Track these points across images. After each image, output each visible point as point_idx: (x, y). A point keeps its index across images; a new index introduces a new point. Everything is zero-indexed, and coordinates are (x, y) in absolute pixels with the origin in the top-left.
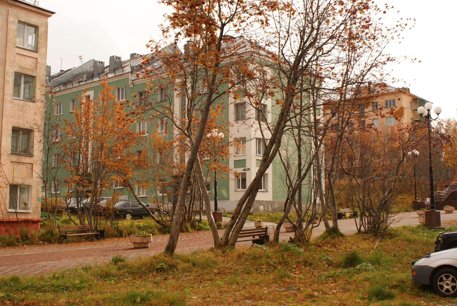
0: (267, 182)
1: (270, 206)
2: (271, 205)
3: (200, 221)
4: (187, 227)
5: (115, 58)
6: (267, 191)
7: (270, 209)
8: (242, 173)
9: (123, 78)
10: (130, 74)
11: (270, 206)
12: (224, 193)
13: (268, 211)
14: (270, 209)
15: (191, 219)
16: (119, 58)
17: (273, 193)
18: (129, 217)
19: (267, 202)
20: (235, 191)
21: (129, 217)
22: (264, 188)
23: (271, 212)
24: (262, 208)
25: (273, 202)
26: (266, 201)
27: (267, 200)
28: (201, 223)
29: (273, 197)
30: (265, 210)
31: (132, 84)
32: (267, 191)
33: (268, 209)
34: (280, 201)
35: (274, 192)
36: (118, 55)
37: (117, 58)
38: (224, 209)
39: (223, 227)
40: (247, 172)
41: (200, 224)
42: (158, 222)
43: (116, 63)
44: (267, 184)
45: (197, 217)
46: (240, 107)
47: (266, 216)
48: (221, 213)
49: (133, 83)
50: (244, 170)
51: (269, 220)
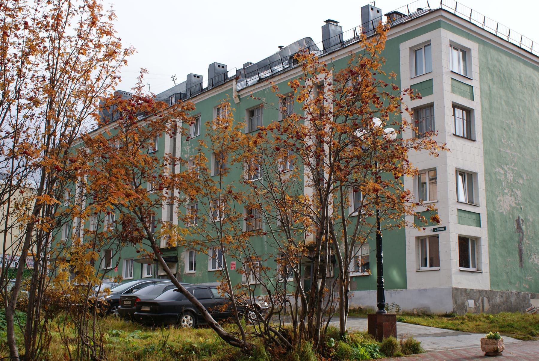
0: (479, 253)
1: (486, 300)
2: (488, 298)
3: (341, 335)
4: (304, 352)
5: (216, 66)
6: (479, 271)
7: (487, 306)
8: (430, 237)
9: (225, 90)
10: (234, 81)
11: (486, 300)
12: (395, 275)
13: (483, 310)
14: (487, 306)
15: (317, 330)
16: (223, 67)
17: (490, 275)
18: (187, 321)
19: (480, 292)
20: (418, 271)
21: (187, 321)
22: (474, 266)
23: (488, 312)
24: (471, 303)
25: (492, 291)
26: (479, 291)
27: (481, 289)
28: (344, 341)
29: (492, 283)
30: (477, 308)
31: (237, 98)
32: (479, 271)
33: (483, 306)
34: (504, 290)
35: (494, 274)
36: (222, 62)
37: (219, 66)
38: (397, 306)
39: (399, 350)
40: (441, 234)
41: (342, 343)
42: (227, 338)
43: (218, 74)
44: (479, 258)
45: (335, 324)
46: (423, 114)
47: (483, 319)
48: (395, 315)
49: (239, 96)
50: (435, 230)
51: (521, 337)
